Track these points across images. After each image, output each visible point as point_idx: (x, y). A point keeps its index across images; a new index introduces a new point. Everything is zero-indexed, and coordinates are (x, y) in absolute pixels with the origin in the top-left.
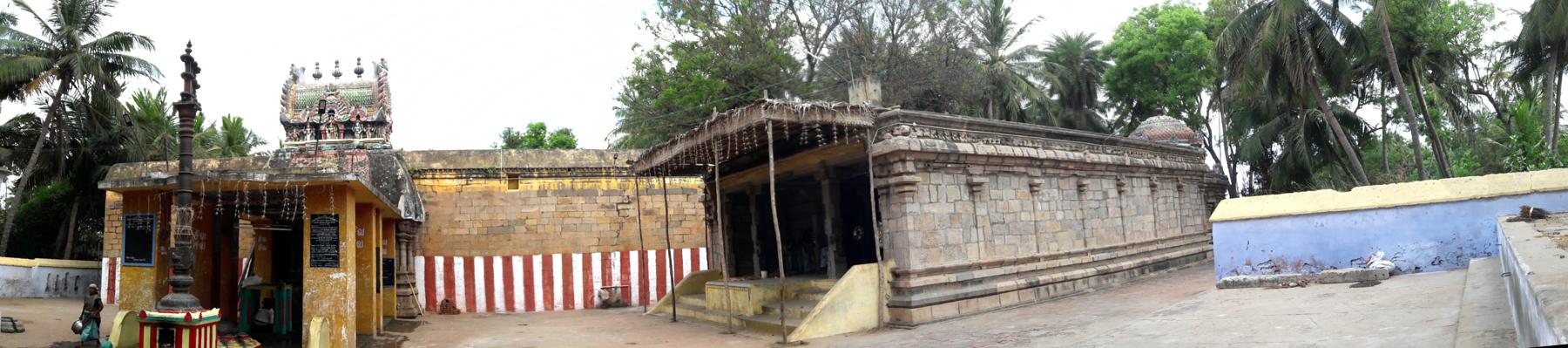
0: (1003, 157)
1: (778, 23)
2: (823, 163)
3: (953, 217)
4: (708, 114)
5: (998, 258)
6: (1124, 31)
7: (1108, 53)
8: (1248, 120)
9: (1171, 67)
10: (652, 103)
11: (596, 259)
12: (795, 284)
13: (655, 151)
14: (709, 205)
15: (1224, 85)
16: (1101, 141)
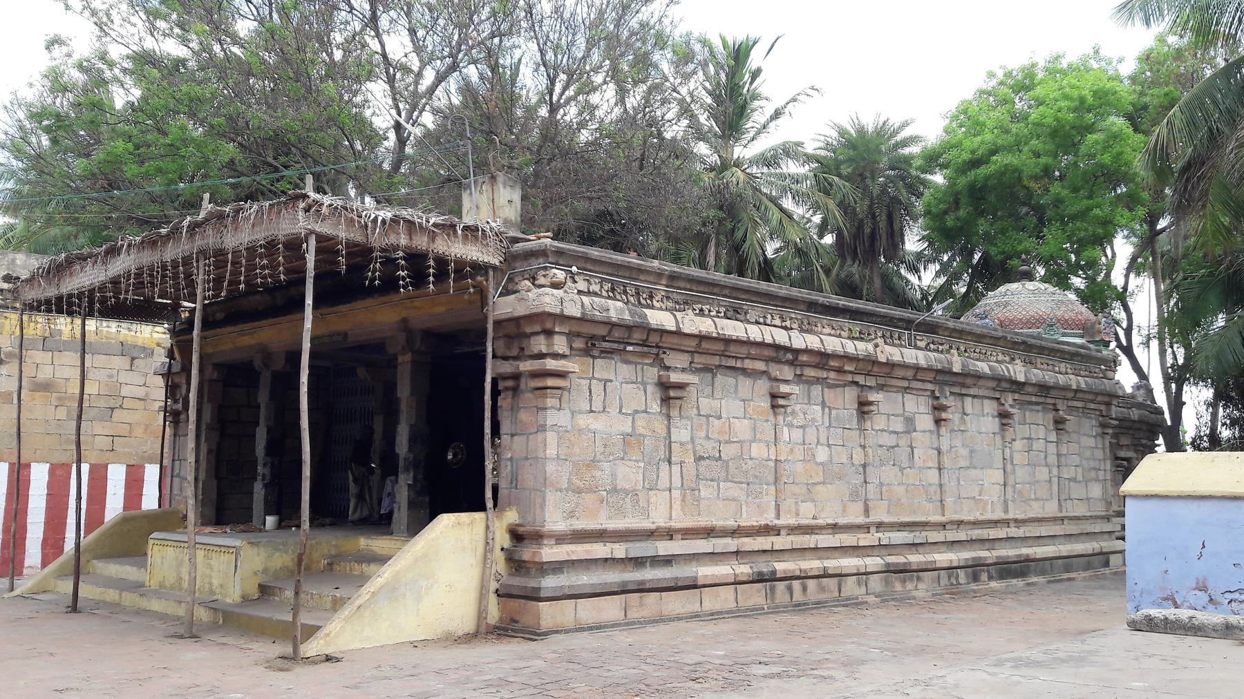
0: (728, 341)
1: (347, 52)
2: (404, 321)
3: (629, 440)
4: (193, 205)
5: (703, 521)
6: (966, 118)
7: (933, 160)
8: (1213, 298)
9: (1056, 188)
10: (79, 165)
12: (329, 542)
13: (69, 262)
14: (174, 384)
15: (1162, 224)
16: (908, 324)
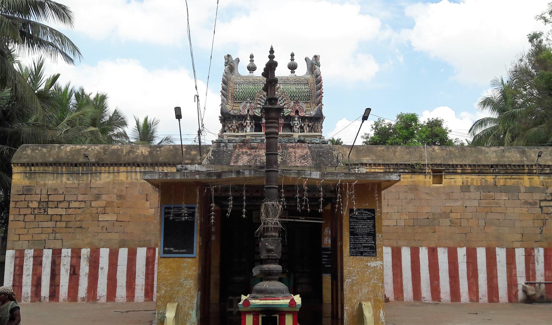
11: (520, 254)
